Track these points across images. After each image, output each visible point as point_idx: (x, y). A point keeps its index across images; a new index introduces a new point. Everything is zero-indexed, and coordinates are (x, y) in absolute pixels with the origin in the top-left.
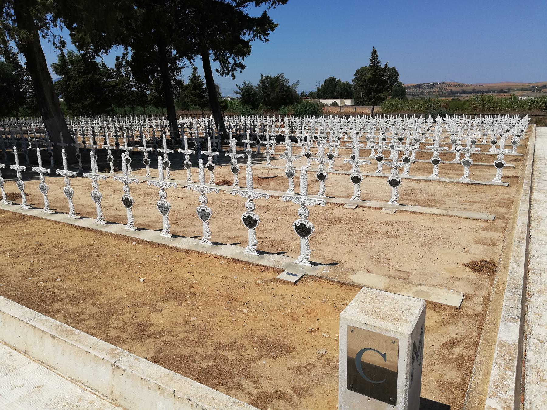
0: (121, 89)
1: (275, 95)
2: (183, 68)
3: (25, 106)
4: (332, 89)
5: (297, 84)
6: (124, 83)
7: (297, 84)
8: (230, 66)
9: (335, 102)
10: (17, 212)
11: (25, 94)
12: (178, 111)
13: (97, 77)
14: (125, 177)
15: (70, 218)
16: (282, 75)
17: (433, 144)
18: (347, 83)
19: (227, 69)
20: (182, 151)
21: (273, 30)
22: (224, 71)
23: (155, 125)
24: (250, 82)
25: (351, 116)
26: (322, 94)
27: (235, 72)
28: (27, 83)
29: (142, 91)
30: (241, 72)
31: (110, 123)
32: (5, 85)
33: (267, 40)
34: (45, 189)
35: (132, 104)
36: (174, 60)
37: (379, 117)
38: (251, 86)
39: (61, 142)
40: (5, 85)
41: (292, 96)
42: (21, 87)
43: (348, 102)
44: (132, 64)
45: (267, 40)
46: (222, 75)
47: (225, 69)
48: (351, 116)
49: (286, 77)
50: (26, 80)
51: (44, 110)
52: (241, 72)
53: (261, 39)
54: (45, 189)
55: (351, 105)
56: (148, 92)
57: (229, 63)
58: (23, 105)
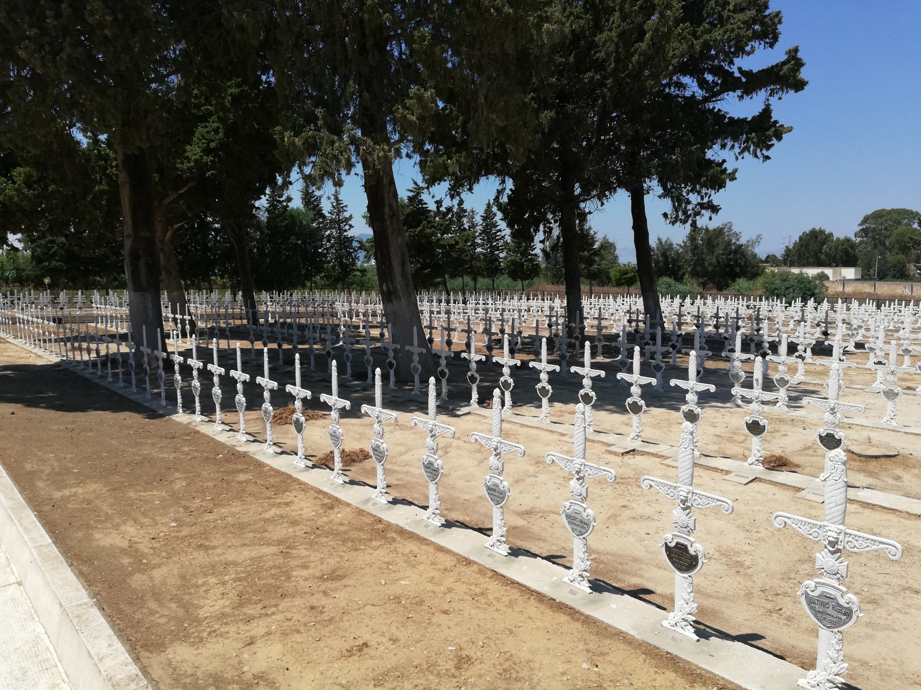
0: (462, 251)
1: (714, 260)
2: (590, 213)
3: (322, 275)
4: (815, 248)
5: (758, 240)
6: (466, 241)
7: (758, 240)
8: (690, 207)
9: (822, 273)
10: (365, 508)
11: (325, 256)
12: (584, 288)
13: (428, 231)
14: (685, 488)
15: (491, 550)
16: (729, 225)
17: (844, 336)
18: (848, 240)
19: (685, 212)
20: (681, 383)
21: (779, 138)
22: (677, 216)
23: (535, 311)
24: (668, 238)
25: (840, 301)
26: (796, 258)
27: (698, 218)
28: (329, 241)
29: (492, 252)
30: (710, 219)
31: (434, 303)
32: (299, 242)
33: (767, 158)
34: (437, 470)
35: (475, 274)
36: (576, 201)
37: (900, 304)
38: (671, 244)
39: (412, 345)
40: (299, 242)
41: (746, 262)
42: (322, 246)
43: (849, 273)
44: (506, 209)
45: (767, 158)
46: (673, 223)
47: (680, 213)
48: (840, 301)
49: (735, 229)
50: (329, 235)
51: (388, 287)
52: (710, 219)
53: (756, 156)
54: (437, 470)
55: (857, 280)
56: (501, 255)
57: (688, 202)
58: (320, 273)
